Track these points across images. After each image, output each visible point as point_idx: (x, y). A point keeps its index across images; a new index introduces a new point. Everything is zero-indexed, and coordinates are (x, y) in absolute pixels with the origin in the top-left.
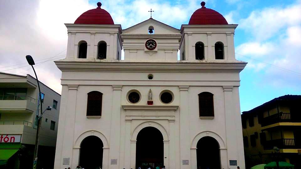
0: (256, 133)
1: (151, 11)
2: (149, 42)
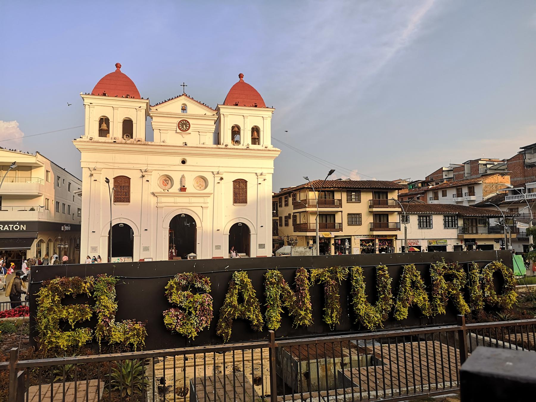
1: (184, 86)
2: (181, 123)
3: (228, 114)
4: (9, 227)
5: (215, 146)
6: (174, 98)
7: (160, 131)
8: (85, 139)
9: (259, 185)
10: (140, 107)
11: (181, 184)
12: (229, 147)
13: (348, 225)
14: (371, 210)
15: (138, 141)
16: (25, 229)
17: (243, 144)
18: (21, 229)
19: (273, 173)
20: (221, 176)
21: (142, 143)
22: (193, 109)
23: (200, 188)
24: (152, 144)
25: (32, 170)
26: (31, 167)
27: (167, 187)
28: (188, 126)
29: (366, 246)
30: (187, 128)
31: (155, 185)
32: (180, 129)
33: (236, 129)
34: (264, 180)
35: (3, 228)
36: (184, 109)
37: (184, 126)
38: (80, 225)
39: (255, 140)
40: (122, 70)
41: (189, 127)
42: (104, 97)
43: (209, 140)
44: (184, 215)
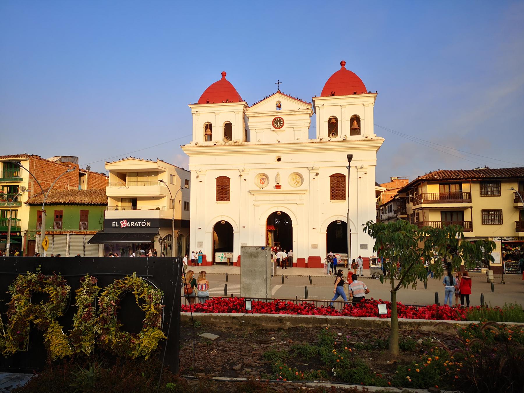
1: (278, 83)
2: (275, 120)
3: (219, 112)
4: (138, 224)
5: (309, 141)
6: (268, 96)
7: (256, 131)
8: (193, 144)
9: (359, 179)
10: (323, 105)
11: (276, 181)
12: (324, 140)
13: (483, 224)
14: (516, 205)
15: (236, 142)
16: (150, 225)
17: (363, 136)
18: (147, 226)
19: (376, 165)
20: (317, 172)
21: (239, 144)
22: (288, 104)
23: (297, 185)
24: (247, 144)
25: (159, 175)
26: (158, 172)
27: (264, 186)
28: (282, 123)
29: (512, 250)
30: (281, 125)
31: (252, 182)
32: (274, 127)
33: (333, 121)
34: (366, 173)
35: (134, 225)
36: (279, 107)
37: (278, 123)
38: (189, 221)
39: (355, 130)
40: (347, 67)
41: (283, 124)
42: (355, 96)
43: (303, 135)
44: (280, 213)
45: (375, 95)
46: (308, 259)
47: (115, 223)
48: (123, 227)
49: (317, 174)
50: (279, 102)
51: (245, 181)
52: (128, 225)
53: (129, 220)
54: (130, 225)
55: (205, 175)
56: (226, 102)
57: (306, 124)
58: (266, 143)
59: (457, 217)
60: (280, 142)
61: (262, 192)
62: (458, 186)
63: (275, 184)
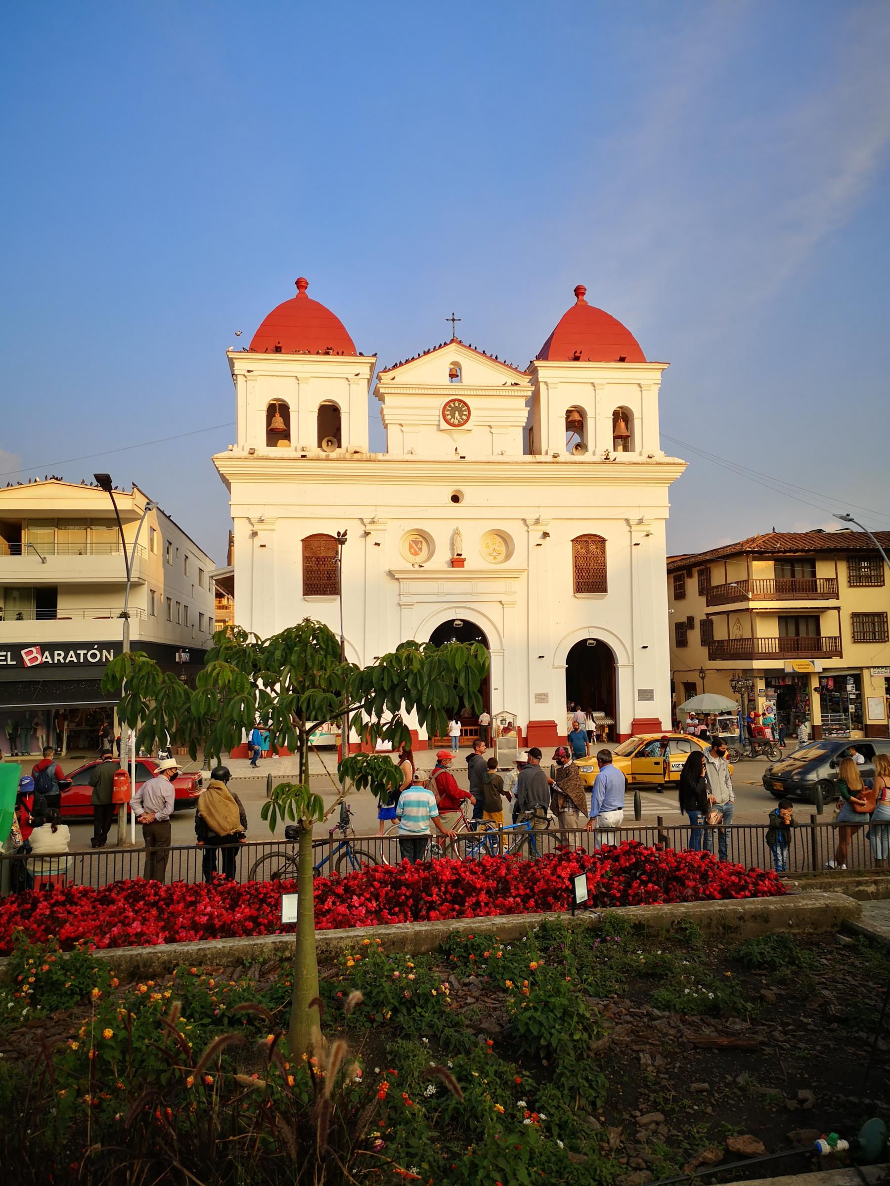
0: (691, 619)
1: (453, 320)
2: (450, 406)
4: (78, 656)
7: (403, 428)
9: (634, 547)
13: (855, 642)
18: (104, 660)
21: (364, 458)
23: (495, 558)
27: (420, 559)
33: (576, 417)
34: (647, 535)
35: (65, 658)
44: (460, 622)
45: (373, 360)
46: (528, 727)
47: (6, 656)
48: (29, 665)
49: (546, 535)
50: (456, 364)
51: (376, 547)
52: (44, 660)
53: (45, 647)
54: (53, 659)
55: (274, 530)
56: (328, 353)
57: (519, 419)
58: (437, 459)
59: (807, 626)
60: (464, 458)
61: (420, 574)
62: (807, 569)
63: (448, 557)
